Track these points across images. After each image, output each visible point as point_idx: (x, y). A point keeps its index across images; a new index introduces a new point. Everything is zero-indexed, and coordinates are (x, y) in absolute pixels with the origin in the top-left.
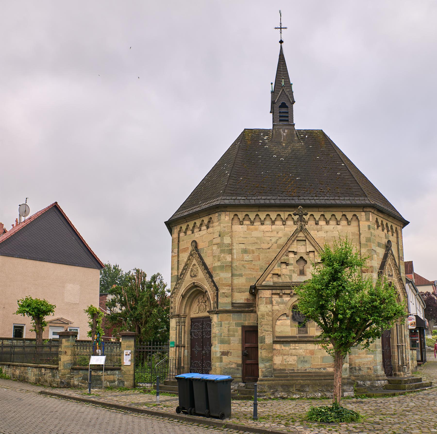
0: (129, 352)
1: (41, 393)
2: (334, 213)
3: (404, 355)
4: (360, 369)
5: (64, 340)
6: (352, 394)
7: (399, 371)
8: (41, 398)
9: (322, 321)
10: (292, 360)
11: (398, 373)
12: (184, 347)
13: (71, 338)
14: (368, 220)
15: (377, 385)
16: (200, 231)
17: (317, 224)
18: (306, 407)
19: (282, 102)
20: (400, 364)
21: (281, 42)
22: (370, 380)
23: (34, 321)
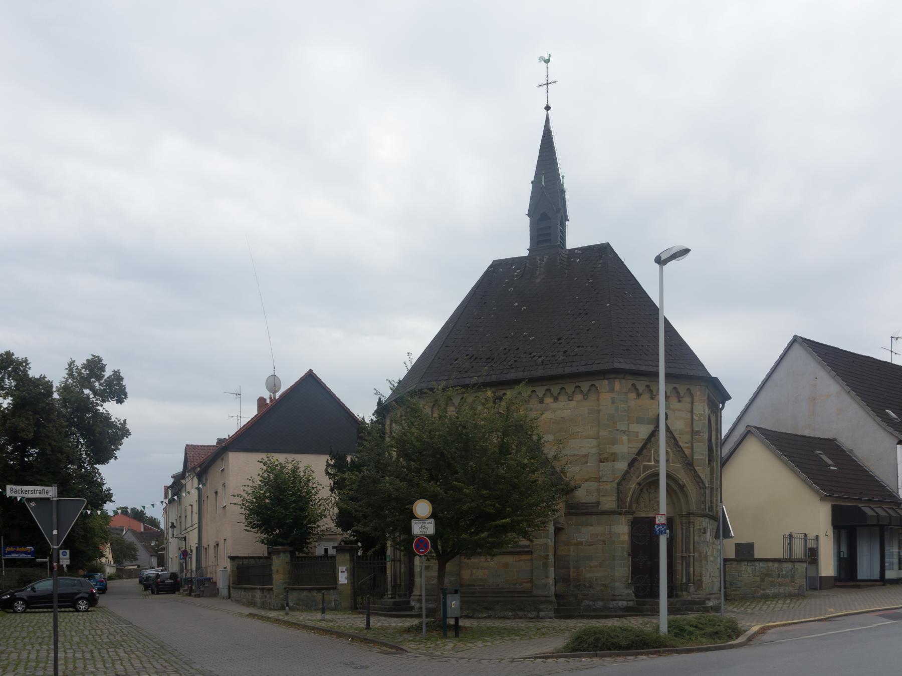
0: (344, 568)
1: (251, 615)
2: (578, 384)
3: (691, 570)
4: (591, 587)
5: (274, 557)
6: (552, 614)
7: (682, 590)
8: (250, 620)
9: (55, 564)
10: (479, 574)
11: (680, 593)
12: (400, 561)
13: (282, 554)
14: (612, 390)
15: (611, 606)
16: (680, 401)
17: (541, 402)
18: (559, 643)
19: (548, 201)
20: (684, 581)
21: (548, 108)
22: (602, 600)
23: (373, 418)
